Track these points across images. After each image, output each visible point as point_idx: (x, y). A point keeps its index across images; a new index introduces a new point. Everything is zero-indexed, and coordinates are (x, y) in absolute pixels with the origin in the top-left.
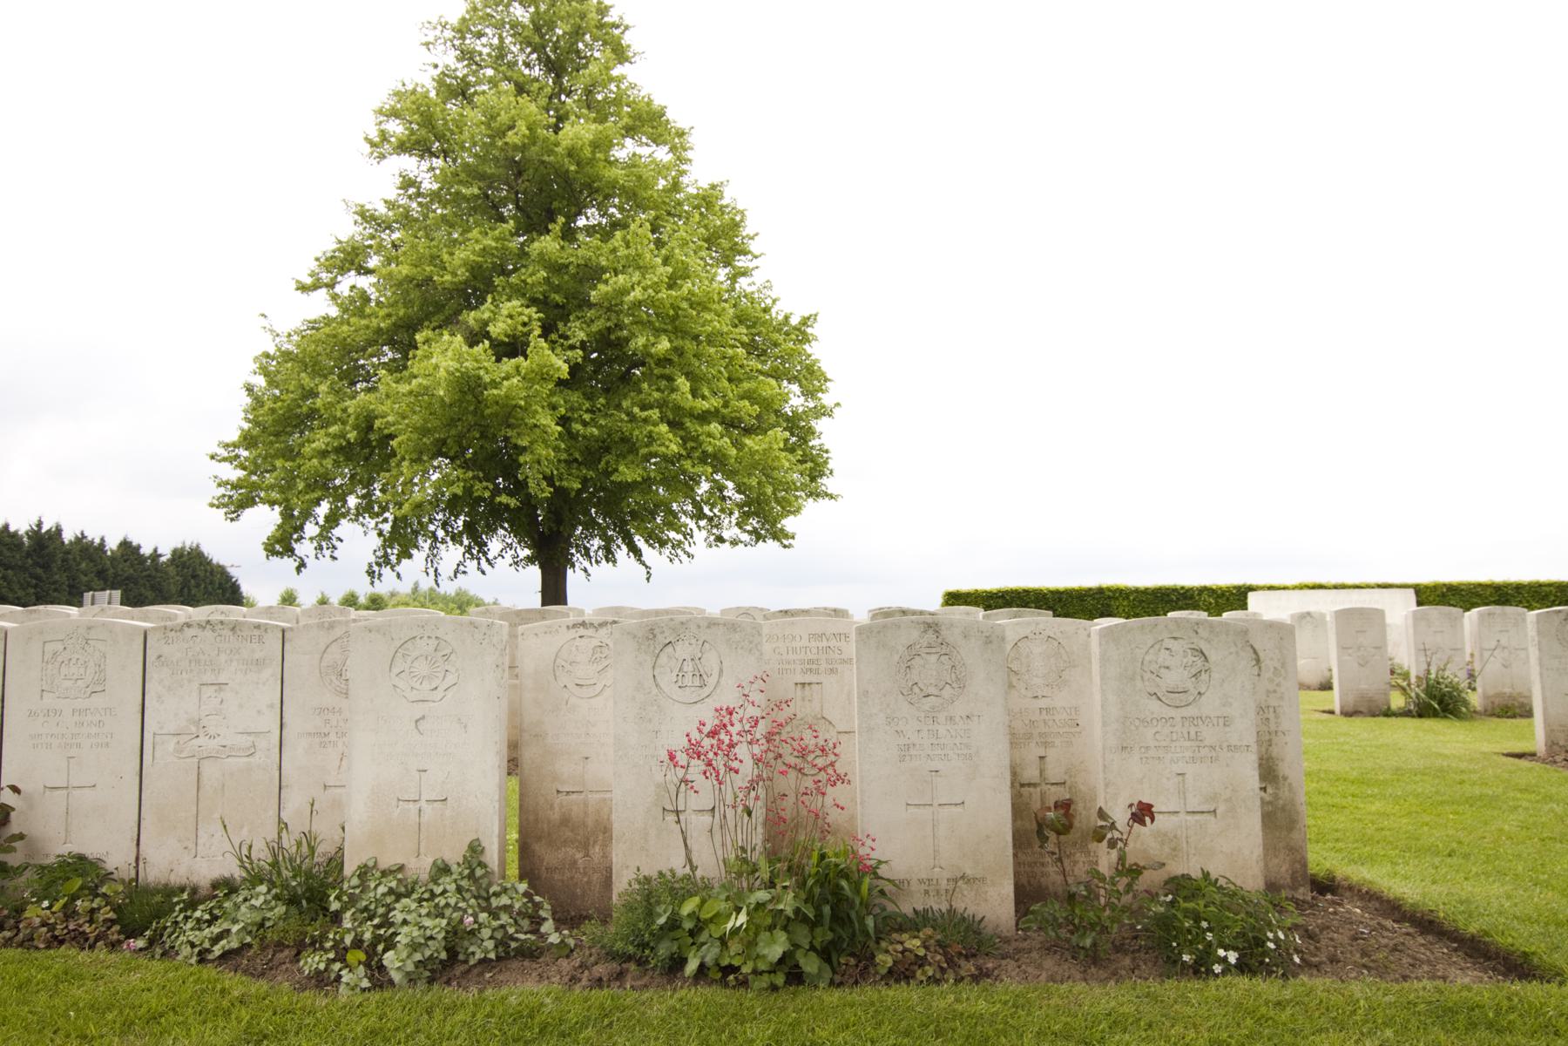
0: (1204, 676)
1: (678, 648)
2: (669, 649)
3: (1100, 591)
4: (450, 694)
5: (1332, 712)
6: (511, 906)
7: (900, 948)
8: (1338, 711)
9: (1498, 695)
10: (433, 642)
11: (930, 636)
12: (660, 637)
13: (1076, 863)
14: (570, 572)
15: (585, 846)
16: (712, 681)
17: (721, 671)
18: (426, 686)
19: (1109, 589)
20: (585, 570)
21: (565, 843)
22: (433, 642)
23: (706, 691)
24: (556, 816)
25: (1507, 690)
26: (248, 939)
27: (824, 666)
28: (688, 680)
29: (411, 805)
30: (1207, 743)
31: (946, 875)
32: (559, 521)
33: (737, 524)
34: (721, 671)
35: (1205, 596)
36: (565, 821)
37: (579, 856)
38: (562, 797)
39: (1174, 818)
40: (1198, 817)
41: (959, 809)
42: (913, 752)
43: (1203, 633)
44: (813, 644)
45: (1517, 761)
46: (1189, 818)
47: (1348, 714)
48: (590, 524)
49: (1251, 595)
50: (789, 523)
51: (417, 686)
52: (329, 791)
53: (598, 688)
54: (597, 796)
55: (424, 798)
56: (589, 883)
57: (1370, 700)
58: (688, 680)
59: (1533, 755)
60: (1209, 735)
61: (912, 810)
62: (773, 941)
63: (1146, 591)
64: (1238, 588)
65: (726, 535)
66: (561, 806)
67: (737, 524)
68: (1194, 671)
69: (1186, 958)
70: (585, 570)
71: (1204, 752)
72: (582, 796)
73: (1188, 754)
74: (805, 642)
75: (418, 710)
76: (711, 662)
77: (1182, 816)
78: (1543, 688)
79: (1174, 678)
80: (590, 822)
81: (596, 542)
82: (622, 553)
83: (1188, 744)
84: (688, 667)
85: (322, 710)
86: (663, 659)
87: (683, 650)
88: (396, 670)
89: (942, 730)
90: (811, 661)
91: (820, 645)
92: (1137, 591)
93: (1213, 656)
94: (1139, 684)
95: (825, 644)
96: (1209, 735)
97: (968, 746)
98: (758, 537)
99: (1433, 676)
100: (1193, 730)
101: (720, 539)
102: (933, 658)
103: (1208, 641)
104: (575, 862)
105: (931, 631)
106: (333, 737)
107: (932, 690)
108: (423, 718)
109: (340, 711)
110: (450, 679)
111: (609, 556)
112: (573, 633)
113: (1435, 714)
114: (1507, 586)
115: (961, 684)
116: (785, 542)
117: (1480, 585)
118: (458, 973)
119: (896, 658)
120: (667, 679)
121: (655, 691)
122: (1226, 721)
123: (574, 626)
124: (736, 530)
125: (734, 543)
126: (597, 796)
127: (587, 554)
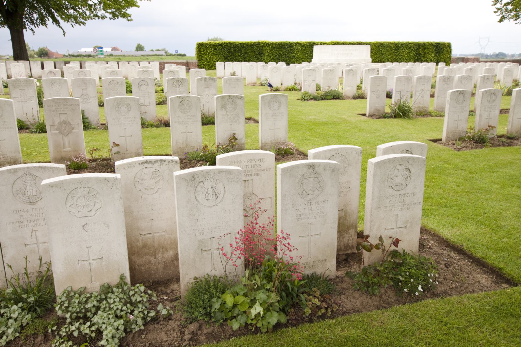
0: (409, 179)
1: (205, 183)
2: (202, 184)
3: (259, 43)
4: (98, 213)
5: (364, 115)
6: (143, 300)
7: (311, 303)
8: (367, 115)
9: (419, 107)
10: (87, 190)
11: (311, 170)
12: (197, 179)
13: (344, 237)
14: (24, 30)
15: (154, 255)
16: (220, 196)
17: (225, 191)
18: (86, 210)
19: (262, 43)
20: (32, 30)
21: (145, 254)
22: (87, 190)
23: (219, 200)
24: (140, 244)
25: (421, 105)
26: (18, 335)
27: (254, 173)
28: (211, 197)
29: (85, 262)
30: (406, 203)
31: (313, 260)
32: (16, 6)
33: (103, 9)
34: (225, 191)
35: (297, 46)
36: (145, 246)
37: (152, 259)
38: (143, 236)
39: (393, 231)
40: (400, 229)
41: (318, 236)
42: (302, 217)
43: (410, 162)
44: (250, 164)
45: (435, 144)
46: (397, 230)
47: (371, 116)
48: (33, 8)
49: (315, 47)
50: (130, 11)
51: (81, 210)
52: (28, 247)
53: (156, 190)
54: (158, 234)
55: (91, 258)
56: (157, 268)
57: (379, 111)
58: (211, 197)
59: (441, 140)
60: (408, 200)
61: (301, 238)
62: (272, 316)
63: (276, 44)
64: (310, 43)
65: (99, 14)
66: (142, 240)
67: (103, 9)
68: (405, 177)
69: (406, 290)
70: (32, 30)
71: (406, 206)
72: (151, 235)
73: (400, 208)
74: (246, 163)
75: (83, 221)
76: (220, 187)
77: (395, 229)
78: (448, 118)
79: (398, 180)
80: (156, 245)
81: (35, 16)
82: (49, 21)
83: (400, 204)
84: (211, 191)
85: (17, 211)
86: (199, 188)
87: (208, 184)
88: (69, 204)
89: (314, 207)
90: (248, 171)
91: (252, 164)
92: (273, 44)
93: (412, 171)
94: (386, 183)
95: (254, 163)
96: (408, 200)
97: (323, 212)
98: (115, 16)
99: (402, 103)
100: (403, 198)
101: (97, 16)
102: (312, 179)
103: (412, 165)
104: (150, 261)
105: (311, 168)
106: (25, 223)
107: (311, 192)
108: (86, 224)
109: (27, 211)
110: (98, 206)
111: (43, 22)
112: (142, 166)
113: (401, 117)
114: (399, 43)
115: (321, 188)
116: (129, 18)
117: (390, 43)
118: (130, 339)
119: (297, 180)
120: (201, 197)
121: (196, 202)
122: (414, 194)
123: (142, 163)
124: (103, 12)
125: (103, 18)
126: (158, 234)
127: (32, 22)
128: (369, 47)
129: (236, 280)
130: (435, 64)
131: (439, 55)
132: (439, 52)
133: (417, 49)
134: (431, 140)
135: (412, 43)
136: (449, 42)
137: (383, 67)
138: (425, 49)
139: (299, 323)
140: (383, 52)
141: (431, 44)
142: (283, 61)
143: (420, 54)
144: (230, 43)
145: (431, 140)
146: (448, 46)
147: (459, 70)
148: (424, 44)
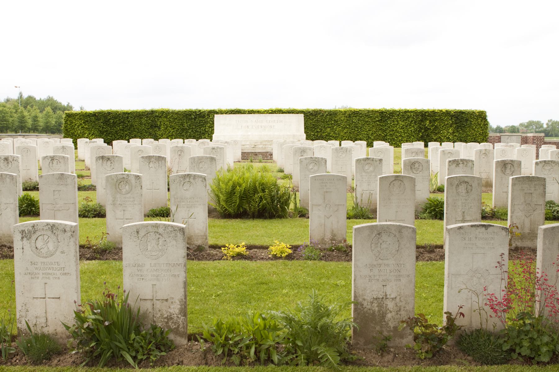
49: (217, 118)
128: (302, 116)
129: (169, 314)
130: (364, 143)
131: (464, 131)
132: (467, 125)
133: (422, 121)
134: (63, 324)
135: (411, 112)
136: (482, 109)
137: (324, 149)
138: (435, 121)
139: (157, 366)
140: (320, 124)
141: (448, 113)
142: (135, 137)
143: (426, 129)
144: (109, 113)
145: (63, 324)
146: (482, 116)
147: (501, 151)
148: (434, 112)
